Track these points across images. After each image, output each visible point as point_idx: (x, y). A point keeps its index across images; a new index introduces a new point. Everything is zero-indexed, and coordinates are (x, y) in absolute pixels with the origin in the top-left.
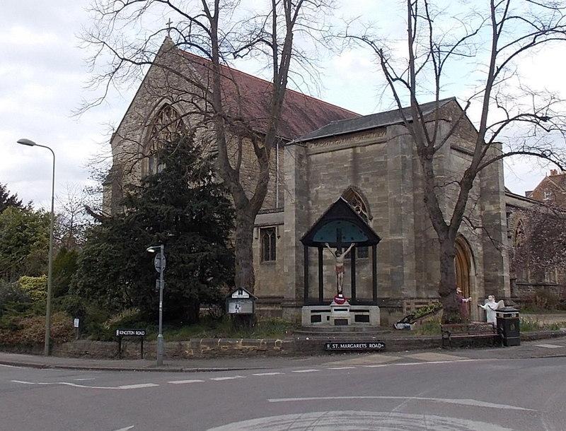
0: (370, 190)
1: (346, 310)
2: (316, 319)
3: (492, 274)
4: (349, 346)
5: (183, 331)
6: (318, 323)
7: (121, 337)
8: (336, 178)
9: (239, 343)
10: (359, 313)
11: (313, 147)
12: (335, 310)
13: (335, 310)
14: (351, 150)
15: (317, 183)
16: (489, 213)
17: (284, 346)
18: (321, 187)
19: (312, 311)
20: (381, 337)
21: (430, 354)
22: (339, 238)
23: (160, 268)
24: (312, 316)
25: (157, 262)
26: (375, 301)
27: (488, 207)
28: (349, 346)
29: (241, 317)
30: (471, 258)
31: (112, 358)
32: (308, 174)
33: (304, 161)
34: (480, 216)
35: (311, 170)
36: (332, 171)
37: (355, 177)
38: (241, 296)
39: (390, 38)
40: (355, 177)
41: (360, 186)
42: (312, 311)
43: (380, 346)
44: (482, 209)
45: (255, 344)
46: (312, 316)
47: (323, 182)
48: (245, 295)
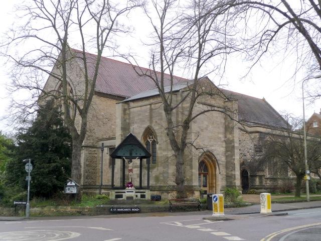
0: (157, 128)
1: (133, 192)
2: (117, 197)
3: (230, 173)
4: (122, 210)
5: (44, 203)
6: (121, 199)
7: (16, 205)
8: (142, 121)
9: (69, 209)
10: (142, 194)
11: (132, 104)
12: (127, 192)
13: (127, 192)
14: (149, 106)
15: (133, 123)
16: (229, 139)
17: (90, 210)
18: (135, 126)
19: (116, 193)
20: (139, 206)
21: (139, 218)
22: (131, 154)
23: (28, 170)
24: (116, 195)
25: (26, 167)
26: (148, 188)
27: (229, 136)
28: (122, 210)
29: (73, 195)
30: (217, 164)
31: (12, 216)
32: (129, 119)
33: (127, 112)
34: (225, 141)
35: (131, 116)
36: (140, 117)
37: (151, 122)
38: (71, 185)
39: (240, 55)
40: (151, 122)
41: (153, 125)
42: (116, 193)
43: (137, 210)
44: (225, 137)
45: (77, 209)
46: (116, 195)
47: (136, 123)
48: (73, 184)
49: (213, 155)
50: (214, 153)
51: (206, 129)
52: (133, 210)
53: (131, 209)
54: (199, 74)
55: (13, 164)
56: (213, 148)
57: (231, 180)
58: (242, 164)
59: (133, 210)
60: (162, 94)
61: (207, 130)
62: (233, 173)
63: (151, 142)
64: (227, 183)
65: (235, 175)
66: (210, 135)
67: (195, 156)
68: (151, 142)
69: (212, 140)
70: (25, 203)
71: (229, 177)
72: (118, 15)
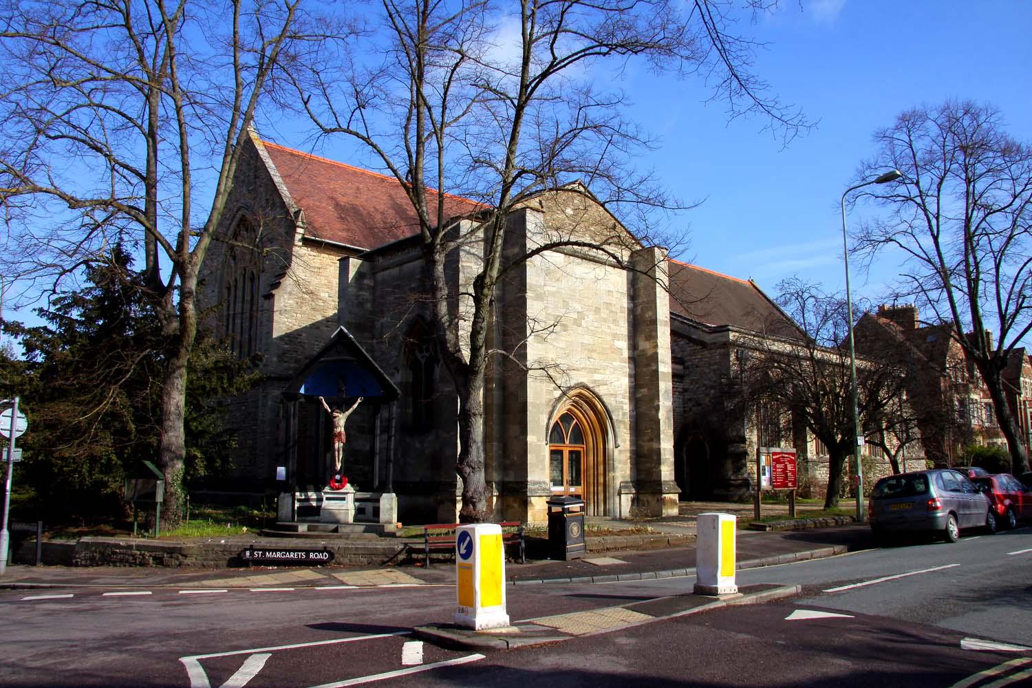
43: (325, 556)
49: (611, 419)
50: (601, 391)
51: (577, 323)
52: (312, 556)
53: (308, 552)
54: (1019, 342)
55: (437, 48)
56: (597, 377)
57: (649, 465)
58: (849, 551)
59: (312, 556)
60: (154, 33)
61: (580, 325)
62: (655, 445)
63: (423, 361)
64: (638, 475)
65: (658, 452)
66: (587, 339)
67: (542, 402)
68: (423, 361)
69: (595, 355)
70: (35, 541)
71: (644, 459)
72: (439, 158)
